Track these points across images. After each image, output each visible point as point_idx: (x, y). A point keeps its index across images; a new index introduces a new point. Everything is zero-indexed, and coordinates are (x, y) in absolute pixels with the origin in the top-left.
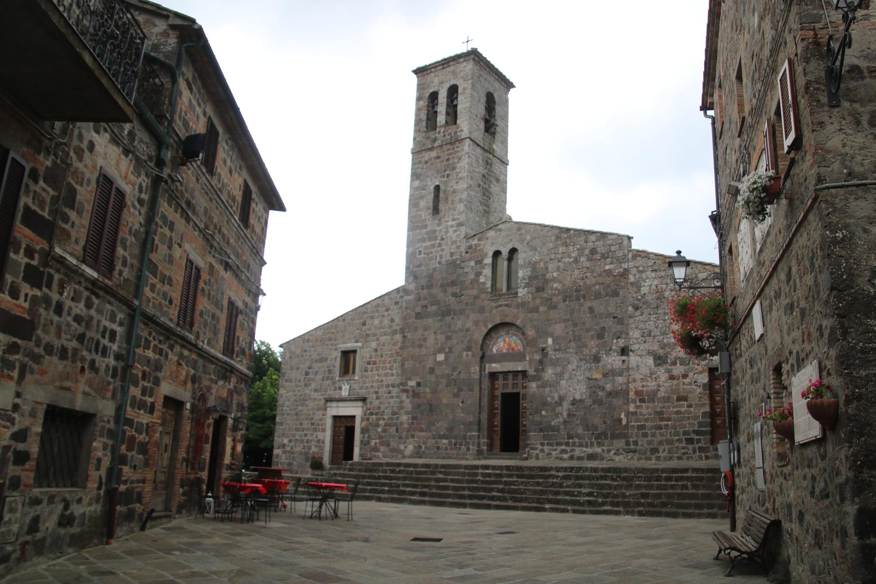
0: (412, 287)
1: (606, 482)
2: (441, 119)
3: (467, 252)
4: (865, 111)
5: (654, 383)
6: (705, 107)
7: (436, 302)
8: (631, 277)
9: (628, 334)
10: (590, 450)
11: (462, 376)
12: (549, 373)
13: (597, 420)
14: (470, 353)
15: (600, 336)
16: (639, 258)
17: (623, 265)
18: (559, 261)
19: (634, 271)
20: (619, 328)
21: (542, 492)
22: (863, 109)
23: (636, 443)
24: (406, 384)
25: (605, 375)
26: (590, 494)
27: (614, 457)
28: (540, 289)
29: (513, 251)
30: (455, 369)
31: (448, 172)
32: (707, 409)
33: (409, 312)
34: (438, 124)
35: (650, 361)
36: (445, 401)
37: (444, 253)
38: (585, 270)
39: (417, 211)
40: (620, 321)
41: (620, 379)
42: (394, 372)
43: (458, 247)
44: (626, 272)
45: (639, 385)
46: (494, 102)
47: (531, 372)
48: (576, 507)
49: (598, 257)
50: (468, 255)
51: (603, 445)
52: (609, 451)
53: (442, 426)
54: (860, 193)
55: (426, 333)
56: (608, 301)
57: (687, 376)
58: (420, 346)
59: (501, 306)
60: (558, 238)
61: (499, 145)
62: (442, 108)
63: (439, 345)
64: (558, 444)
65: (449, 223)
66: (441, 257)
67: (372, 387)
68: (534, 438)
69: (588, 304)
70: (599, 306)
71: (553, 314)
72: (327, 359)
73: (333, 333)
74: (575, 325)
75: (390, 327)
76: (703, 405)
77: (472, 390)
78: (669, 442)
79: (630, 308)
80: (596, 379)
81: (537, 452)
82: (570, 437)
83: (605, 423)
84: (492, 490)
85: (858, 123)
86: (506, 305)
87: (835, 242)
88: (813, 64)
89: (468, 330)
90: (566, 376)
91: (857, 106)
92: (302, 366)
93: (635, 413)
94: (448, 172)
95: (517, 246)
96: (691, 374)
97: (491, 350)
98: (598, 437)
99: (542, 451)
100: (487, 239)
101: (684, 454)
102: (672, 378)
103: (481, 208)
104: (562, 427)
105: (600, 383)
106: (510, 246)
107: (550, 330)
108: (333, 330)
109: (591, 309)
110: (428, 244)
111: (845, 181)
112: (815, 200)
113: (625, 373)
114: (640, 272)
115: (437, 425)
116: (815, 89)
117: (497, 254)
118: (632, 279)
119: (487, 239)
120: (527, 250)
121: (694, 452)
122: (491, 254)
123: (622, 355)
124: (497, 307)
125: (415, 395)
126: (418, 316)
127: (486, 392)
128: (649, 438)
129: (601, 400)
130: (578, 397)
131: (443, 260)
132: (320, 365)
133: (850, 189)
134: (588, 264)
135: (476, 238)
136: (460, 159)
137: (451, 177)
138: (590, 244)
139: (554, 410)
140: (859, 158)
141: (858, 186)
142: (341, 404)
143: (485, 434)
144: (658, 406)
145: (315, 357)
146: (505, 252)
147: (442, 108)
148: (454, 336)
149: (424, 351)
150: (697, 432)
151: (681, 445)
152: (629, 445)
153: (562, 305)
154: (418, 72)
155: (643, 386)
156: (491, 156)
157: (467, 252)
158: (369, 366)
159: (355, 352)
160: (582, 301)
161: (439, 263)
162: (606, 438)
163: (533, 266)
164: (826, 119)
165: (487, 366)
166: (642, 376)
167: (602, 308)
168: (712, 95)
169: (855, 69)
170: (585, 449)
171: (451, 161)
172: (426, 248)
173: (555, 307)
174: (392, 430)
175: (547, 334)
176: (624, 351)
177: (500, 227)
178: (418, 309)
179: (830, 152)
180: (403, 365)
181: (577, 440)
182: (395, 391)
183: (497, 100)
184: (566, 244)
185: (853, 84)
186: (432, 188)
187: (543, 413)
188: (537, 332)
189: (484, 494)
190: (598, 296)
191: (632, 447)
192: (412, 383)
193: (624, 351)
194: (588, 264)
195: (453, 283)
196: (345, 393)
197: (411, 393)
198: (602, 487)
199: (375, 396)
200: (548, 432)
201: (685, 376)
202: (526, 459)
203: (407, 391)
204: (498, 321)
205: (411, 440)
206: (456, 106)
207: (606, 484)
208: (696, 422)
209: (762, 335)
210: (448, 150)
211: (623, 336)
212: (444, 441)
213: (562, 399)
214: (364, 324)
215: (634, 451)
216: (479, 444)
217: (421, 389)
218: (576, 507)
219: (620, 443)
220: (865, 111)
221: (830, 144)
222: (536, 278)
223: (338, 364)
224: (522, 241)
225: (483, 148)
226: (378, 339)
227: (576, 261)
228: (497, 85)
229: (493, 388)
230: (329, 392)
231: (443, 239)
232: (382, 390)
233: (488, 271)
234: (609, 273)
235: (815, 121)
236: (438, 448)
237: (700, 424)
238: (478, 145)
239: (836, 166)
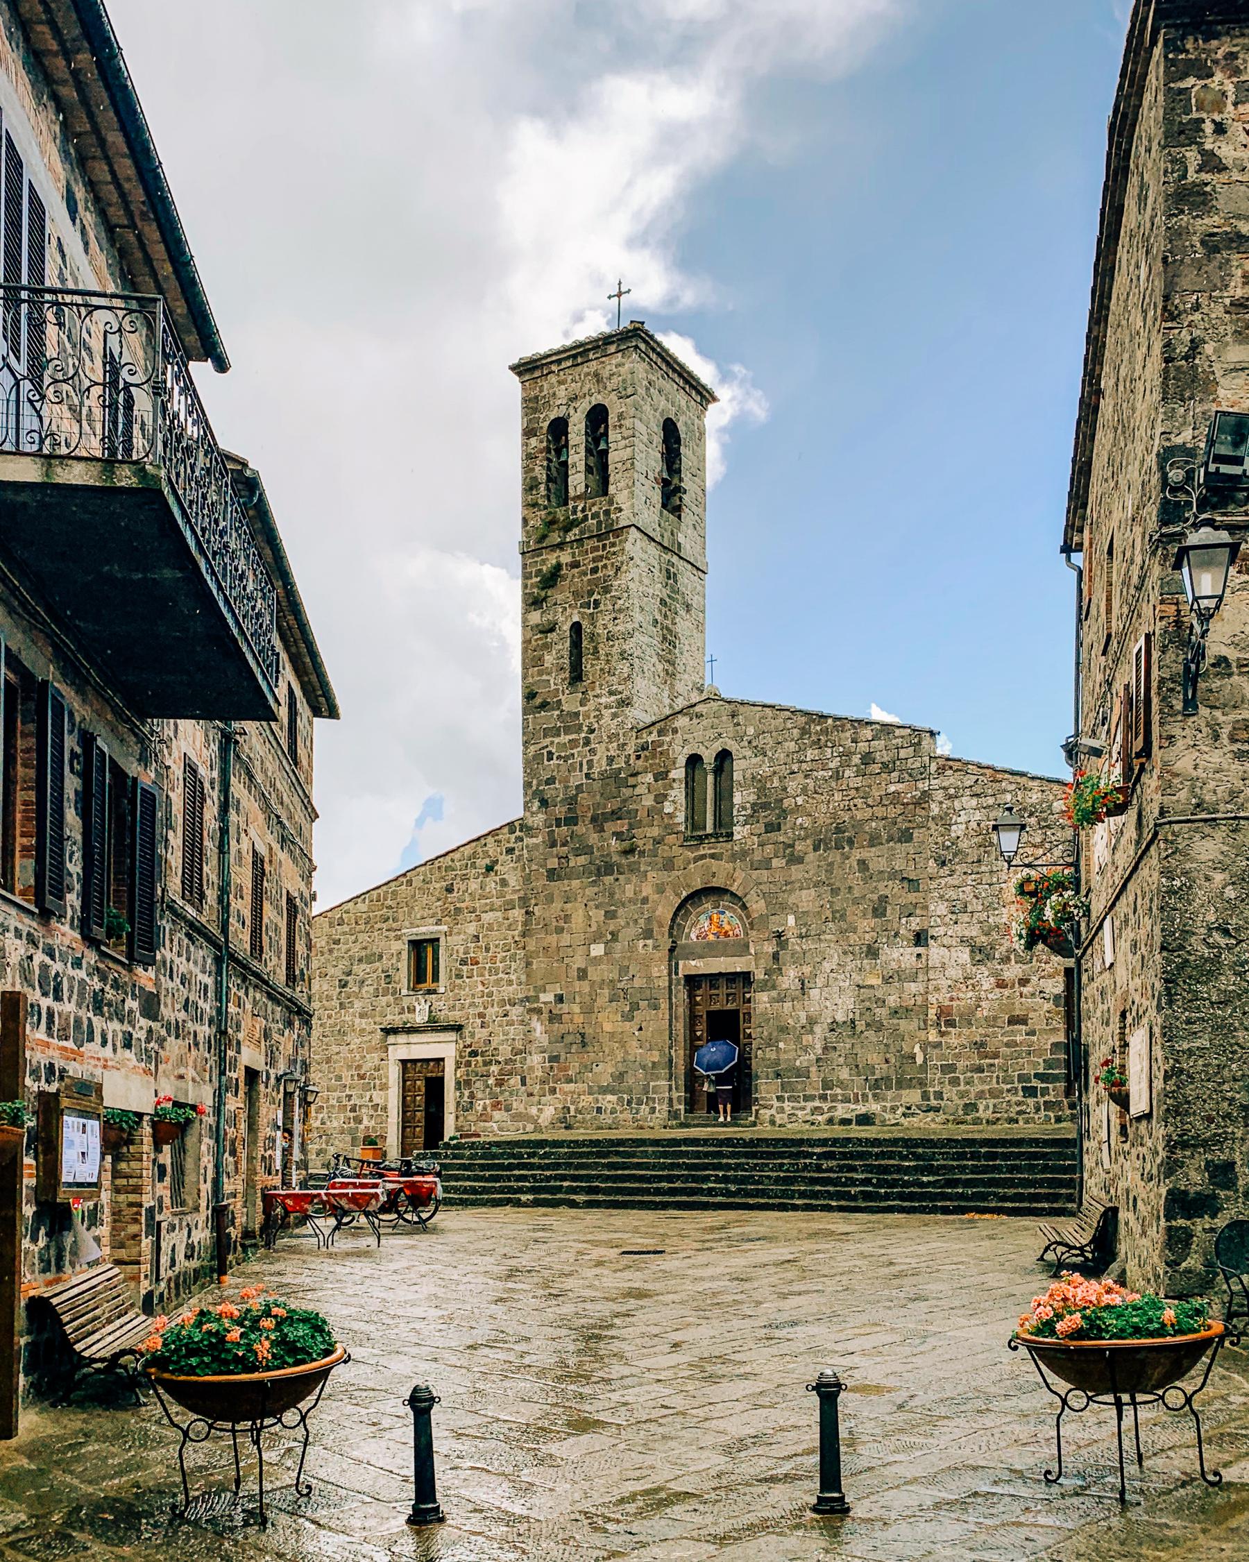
0: (539, 820)
1: (892, 1162)
2: (577, 481)
3: (638, 757)
4: (1226, 720)
5: (970, 994)
6: (1067, 549)
7: (587, 850)
8: (933, 806)
9: (926, 908)
10: (861, 1109)
11: (638, 983)
12: (789, 978)
13: (874, 1058)
14: (650, 942)
15: (879, 911)
16: (950, 772)
17: (920, 785)
18: (806, 777)
19: (939, 795)
20: (912, 897)
21: (786, 1181)
22: (1225, 718)
23: (939, 1095)
24: (537, 997)
25: (887, 980)
26: (867, 1182)
27: (902, 1120)
28: (772, 828)
29: (724, 756)
30: (624, 970)
31: (596, 596)
32: (1061, 1038)
33: (534, 867)
34: (572, 493)
35: (964, 955)
36: (608, 1027)
37: (596, 758)
38: (853, 792)
39: (540, 673)
40: (912, 884)
41: (913, 987)
42: (513, 977)
43: (622, 747)
44: (926, 795)
45: (943, 997)
46: (678, 440)
47: (759, 975)
48: (843, 1203)
49: (876, 768)
50: (640, 762)
51: (884, 1100)
52: (894, 1109)
53: (604, 1072)
54: (1207, 830)
55: (569, 905)
56: (893, 849)
57: (1028, 981)
58: (560, 930)
59: (703, 857)
60: (804, 732)
61: (690, 531)
62: (577, 458)
63: (594, 928)
64: (807, 1098)
65: (603, 700)
66: (590, 763)
67: (472, 1005)
68: (766, 1089)
69: (857, 854)
70: (878, 859)
71: (796, 872)
72: (381, 957)
73: (390, 907)
74: (835, 892)
75: (501, 895)
76: (1055, 1030)
77: (656, 1008)
78: (994, 1094)
79: (931, 862)
80: (872, 987)
81: (773, 1111)
82: (827, 1085)
83: (887, 1061)
84: (706, 1179)
85: (1216, 737)
86: (713, 856)
87: (1171, 892)
88: (1170, 655)
89: (645, 900)
90: (820, 981)
91: (1218, 713)
92: (331, 971)
93: (938, 1045)
94: (596, 596)
95: (732, 746)
96: (1034, 979)
97: (688, 936)
98: (876, 1085)
99: (781, 1111)
100: (675, 731)
101: (1019, 1113)
102: (1001, 984)
103: (660, 667)
104: (813, 1069)
105: (879, 994)
106: (718, 746)
107: (792, 900)
108: (389, 902)
109: (863, 864)
110: (564, 738)
111: (1192, 814)
112: (1156, 834)
113: (921, 977)
114: (950, 797)
115: (595, 1070)
116: (1168, 690)
117: (694, 761)
118: (935, 809)
119: (675, 731)
120: (748, 753)
121: (1038, 1110)
122: (682, 761)
123: (916, 945)
124: (696, 860)
125: (554, 1018)
126: (552, 875)
127: (681, 1010)
128: (962, 1088)
129: (880, 1022)
130: (840, 1018)
131: (596, 770)
132: (368, 968)
133: (1197, 825)
134: (857, 782)
135: (655, 730)
136: (618, 569)
137: (602, 607)
138: (863, 747)
139: (799, 1039)
140: (1212, 784)
141: (1205, 821)
142: (414, 1038)
143: (681, 1083)
144: (977, 1033)
145: (356, 950)
146: (709, 756)
147: (577, 458)
148: (621, 912)
149: (566, 939)
150: (1040, 1077)
151: (1014, 1099)
152: (929, 1100)
153: (811, 857)
154: (527, 369)
155: (952, 999)
156: (675, 559)
157: (638, 757)
158: (465, 968)
159: (434, 941)
160: (847, 849)
161: (588, 776)
162: (889, 1088)
163: (760, 784)
164: (1177, 731)
165: (681, 963)
166: (950, 982)
167: (883, 861)
168: (1081, 530)
169: (1222, 661)
170: (853, 1107)
171: (600, 574)
172: (562, 746)
173: (800, 860)
174: (515, 1081)
175: (784, 908)
176: (920, 938)
177: (697, 709)
178: (553, 863)
179: (1178, 775)
180: (528, 964)
181: (839, 1091)
182: (516, 1012)
183: (682, 436)
184: (817, 744)
185: (1216, 684)
186: (567, 627)
187: (781, 1045)
188: (768, 904)
189: (574, 1197)
190: (874, 841)
191: (934, 1102)
192: (547, 997)
193: (920, 938)
194: (857, 782)
195: (616, 815)
196: (420, 1018)
197: (546, 1015)
198: (886, 1170)
199: (479, 1021)
200: (787, 1076)
201: (1024, 982)
202: (754, 1124)
203: (539, 1011)
204: (698, 885)
205: (548, 1097)
206: (605, 453)
207: (893, 1166)
208: (1041, 1061)
209: (1112, 964)
210: (596, 549)
211: (918, 912)
212: (610, 1097)
213: (812, 1021)
214: (449, 890)
215: (937, 1110)
216: (671, 1100)
217: (565, 1007)
218: (843, 1203)
219: (913, 1096)
220: (1226, 720)
221: (1178, 766)
222: (765, 806)
223: (403, 965)
224: (739, 738)
225: (660, 544)
226: (479, 919)
227: (837, 776)
228: (681, 398)
229: (692, 1004)
230: (389, 1017)
231: (592, 731)
232: (492, 1011)
233: (678, 794)
234: (895, 798)
235: (1164, 734)
236: (599, 1110)
237: (1049, 1064)
238: (652, 539)
239: (1183, 795)
